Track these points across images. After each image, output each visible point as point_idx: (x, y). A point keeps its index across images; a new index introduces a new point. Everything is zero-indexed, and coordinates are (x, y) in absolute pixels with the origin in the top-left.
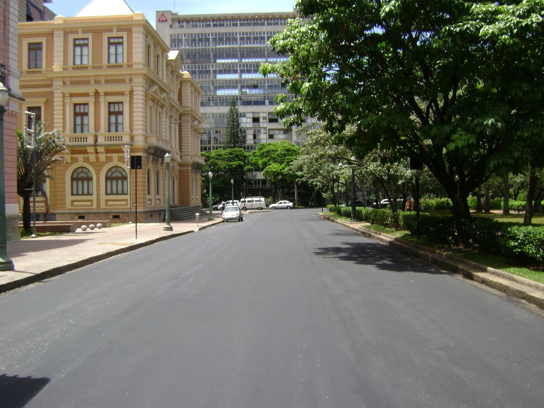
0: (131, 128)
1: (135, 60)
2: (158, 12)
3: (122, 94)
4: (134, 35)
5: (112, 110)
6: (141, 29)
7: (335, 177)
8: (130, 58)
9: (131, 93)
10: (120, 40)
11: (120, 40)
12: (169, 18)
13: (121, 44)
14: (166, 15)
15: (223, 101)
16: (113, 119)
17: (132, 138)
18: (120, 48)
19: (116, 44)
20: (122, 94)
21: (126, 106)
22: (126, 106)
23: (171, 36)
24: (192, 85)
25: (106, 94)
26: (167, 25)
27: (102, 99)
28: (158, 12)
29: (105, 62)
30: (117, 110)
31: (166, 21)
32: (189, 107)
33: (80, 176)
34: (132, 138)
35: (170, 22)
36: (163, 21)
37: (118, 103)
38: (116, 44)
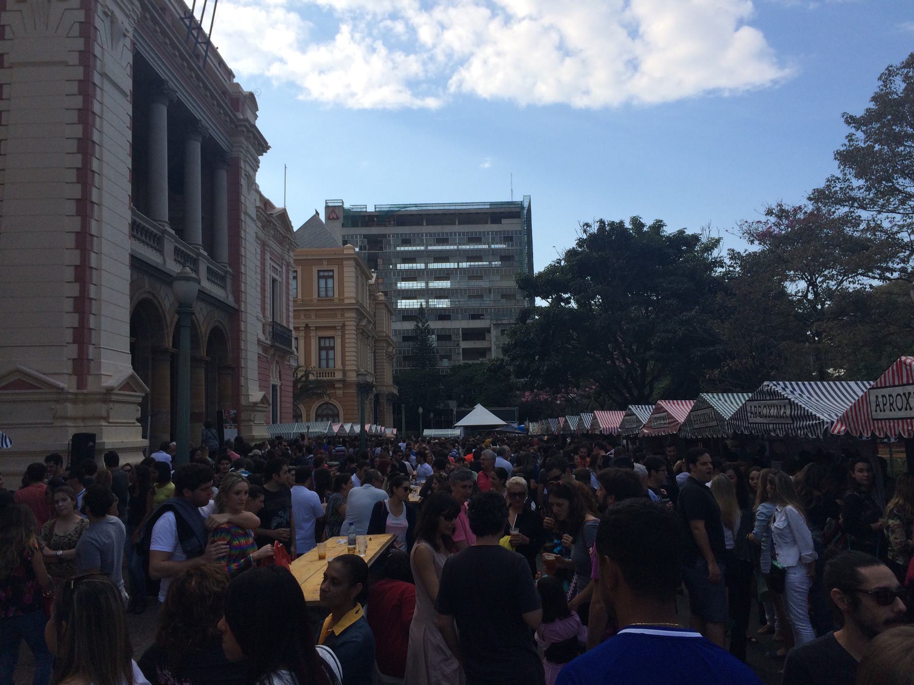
0: (343, 364)
1: (346, 295)
2: (268, 148)
3: (334, 328)
4: (346, 269)
5: (322, 344)
6: (352, 263)
7: (872, 224)
8: (341, 292)
9: (344, 326)
10: (331, 274)
11: (331, 274)
12: (341, 215)
13: (332, 277)
14: (337, 211)
15: (407, 315)
16: (324, 353)
17: (344, 372)
18: (330, 282)
19: (326, 278)
20: (334, 328)
21: (338, 341)
22: (338, 341)
23: (344, 236)
24: (386, 306)
25: (317, 328)
26: (338, 224)
27: (313, 334)
28: (268, 148)
29: (315, 296)
30: (327, 345)
31: (338, 218)
32: (383, 332)
33: (325, 412)
34: (344, 372)
35: (342, 220)
36: (333, 219)
37: (329, 338)
38: (326, 278)
